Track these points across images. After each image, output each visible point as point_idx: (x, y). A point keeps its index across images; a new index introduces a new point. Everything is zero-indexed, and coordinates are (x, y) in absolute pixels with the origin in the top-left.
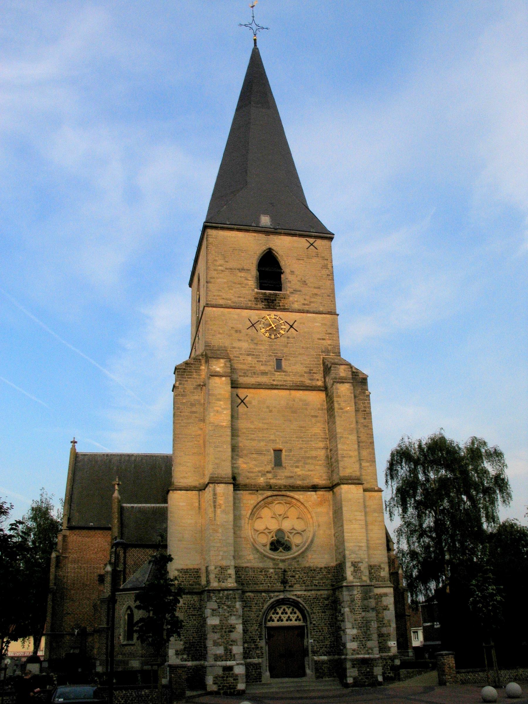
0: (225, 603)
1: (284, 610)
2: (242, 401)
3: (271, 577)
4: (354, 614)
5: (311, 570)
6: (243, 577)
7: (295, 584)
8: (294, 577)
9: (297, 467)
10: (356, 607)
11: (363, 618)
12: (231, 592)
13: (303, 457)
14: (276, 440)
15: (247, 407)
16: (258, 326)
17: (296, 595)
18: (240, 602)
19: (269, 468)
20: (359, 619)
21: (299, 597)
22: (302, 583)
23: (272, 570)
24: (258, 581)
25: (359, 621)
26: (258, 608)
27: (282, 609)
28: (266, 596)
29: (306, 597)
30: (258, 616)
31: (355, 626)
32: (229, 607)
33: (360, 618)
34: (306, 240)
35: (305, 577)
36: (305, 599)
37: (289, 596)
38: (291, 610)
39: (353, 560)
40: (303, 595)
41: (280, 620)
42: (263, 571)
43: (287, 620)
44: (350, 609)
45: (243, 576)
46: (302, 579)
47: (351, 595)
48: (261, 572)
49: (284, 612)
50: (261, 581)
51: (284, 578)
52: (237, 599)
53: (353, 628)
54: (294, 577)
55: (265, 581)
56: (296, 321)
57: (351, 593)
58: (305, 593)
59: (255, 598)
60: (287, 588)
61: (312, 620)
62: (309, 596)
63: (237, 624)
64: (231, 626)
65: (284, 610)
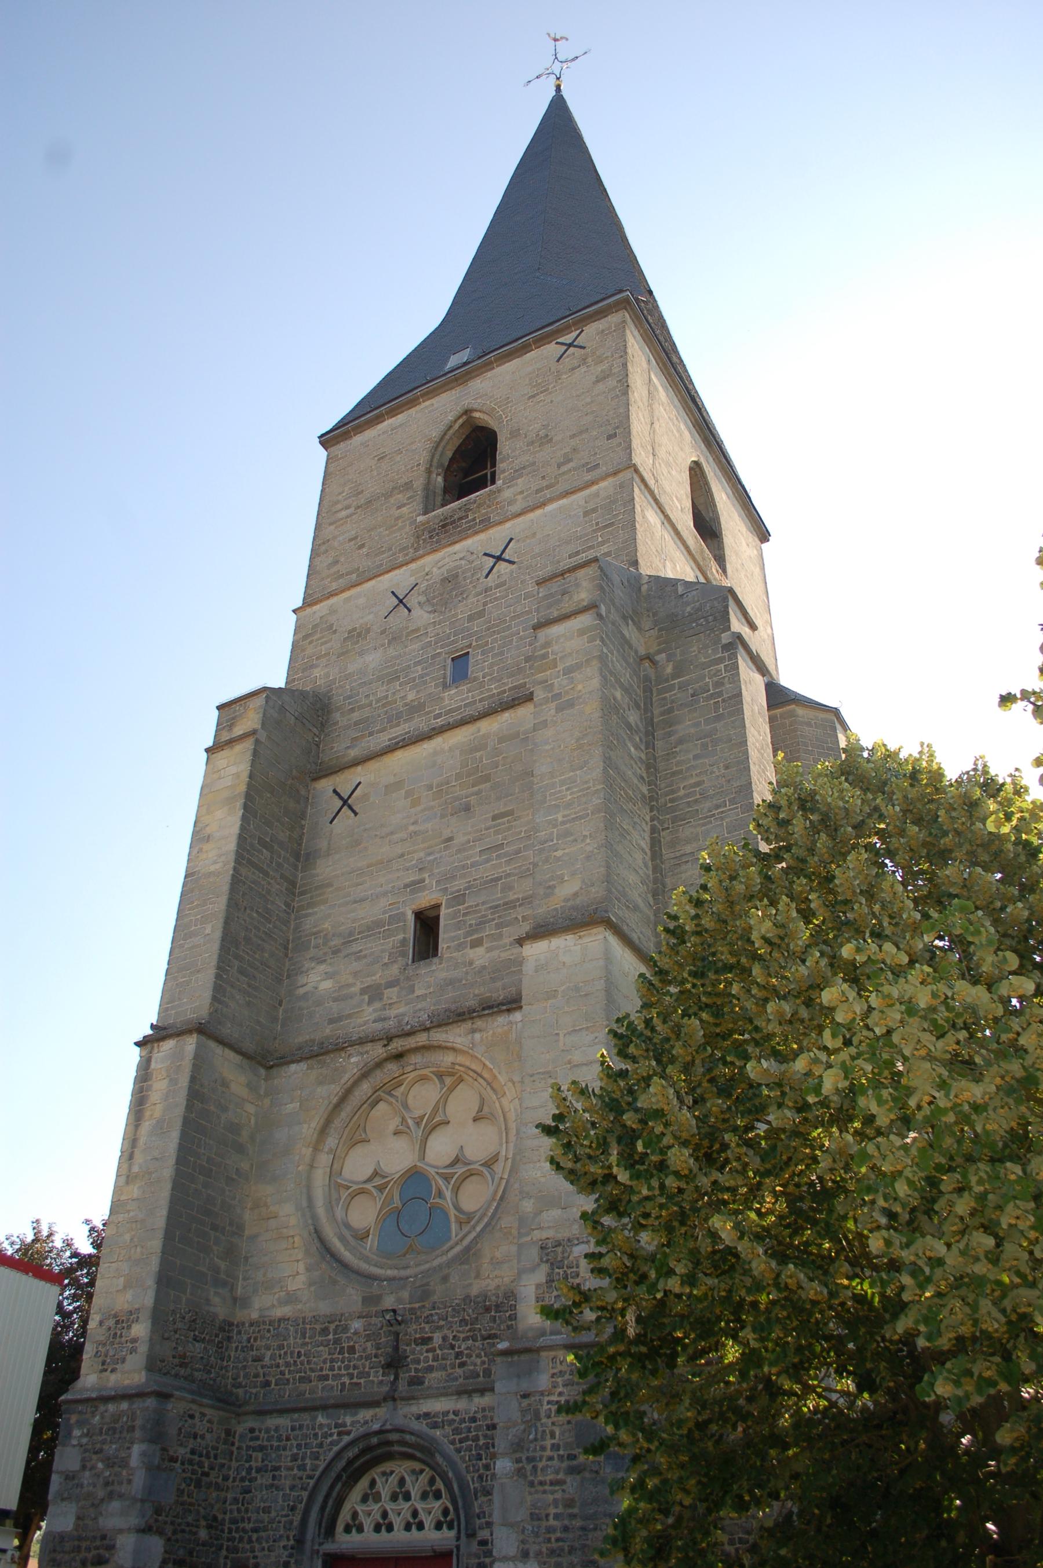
0: (101, 1451)
1: (402, 1482)
2: (345, 802)
3: (352, 1350)
4: (532, 1484)
5: (488, 1309)
6: (267, 1359)
7: (430, 1369)
8: (426, 1341)
9: (477, 943)
10: (543, 1448)
11: (569, 1503)
12: (124, 1405)
13: (497, 907)
14: (423, 880)
15: (356, 814)
16: (412, 601)
17: (427, 1415)
18: (143, 1441)
19: (395, 970)
20: (552, 1511)
21: (435, 1426)
22: (453, 1367)
23: (357, 1325)
24: (312, 1370)
25: (552, 1522)
26: (299, 1474)
27: (393, 1480)
28: (329, 1426)
29: (463, 1421)
30: (293, 1509)
31: (533, 1549)
32: (110, 1463)
33: (556, 1502)
34: (557, 343)
35: (465, 1339)
36: (457, 1431)
37: (400, 1421)
38: (424, 1478)
39: (545, 1234)
40: (451, 1416)
41: (384, 1525)
42: (332, 1327)
43: (377, 1528)
44: (518, 1461)
45: (269, 1353)
46: (452, 1347)
47: (525, 1396)
48: (325, 1331)
49: (401, 1494)
50: (321, 1369)
51: (396, 1348)
52: (138, 1434)
53: (525, 1555)
54: (426, 1341)
55: (332, 1369)
56: (511, 539)
57: (525, 1386)
58: (462, 1404)
59: (292, 1434)
60: (402, 1386)
61: (478, 1522)
62: (473, 1419)
63: (121, 1531)
64: (104, 1537)
65: (402, 1482)
